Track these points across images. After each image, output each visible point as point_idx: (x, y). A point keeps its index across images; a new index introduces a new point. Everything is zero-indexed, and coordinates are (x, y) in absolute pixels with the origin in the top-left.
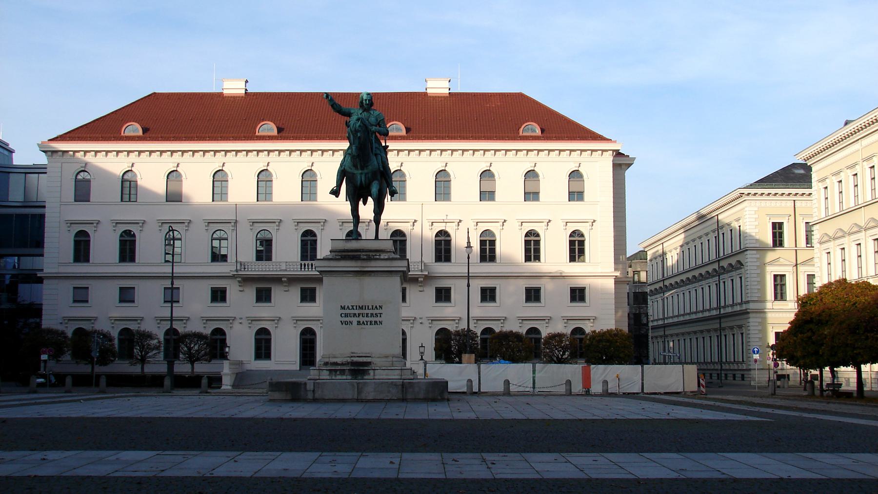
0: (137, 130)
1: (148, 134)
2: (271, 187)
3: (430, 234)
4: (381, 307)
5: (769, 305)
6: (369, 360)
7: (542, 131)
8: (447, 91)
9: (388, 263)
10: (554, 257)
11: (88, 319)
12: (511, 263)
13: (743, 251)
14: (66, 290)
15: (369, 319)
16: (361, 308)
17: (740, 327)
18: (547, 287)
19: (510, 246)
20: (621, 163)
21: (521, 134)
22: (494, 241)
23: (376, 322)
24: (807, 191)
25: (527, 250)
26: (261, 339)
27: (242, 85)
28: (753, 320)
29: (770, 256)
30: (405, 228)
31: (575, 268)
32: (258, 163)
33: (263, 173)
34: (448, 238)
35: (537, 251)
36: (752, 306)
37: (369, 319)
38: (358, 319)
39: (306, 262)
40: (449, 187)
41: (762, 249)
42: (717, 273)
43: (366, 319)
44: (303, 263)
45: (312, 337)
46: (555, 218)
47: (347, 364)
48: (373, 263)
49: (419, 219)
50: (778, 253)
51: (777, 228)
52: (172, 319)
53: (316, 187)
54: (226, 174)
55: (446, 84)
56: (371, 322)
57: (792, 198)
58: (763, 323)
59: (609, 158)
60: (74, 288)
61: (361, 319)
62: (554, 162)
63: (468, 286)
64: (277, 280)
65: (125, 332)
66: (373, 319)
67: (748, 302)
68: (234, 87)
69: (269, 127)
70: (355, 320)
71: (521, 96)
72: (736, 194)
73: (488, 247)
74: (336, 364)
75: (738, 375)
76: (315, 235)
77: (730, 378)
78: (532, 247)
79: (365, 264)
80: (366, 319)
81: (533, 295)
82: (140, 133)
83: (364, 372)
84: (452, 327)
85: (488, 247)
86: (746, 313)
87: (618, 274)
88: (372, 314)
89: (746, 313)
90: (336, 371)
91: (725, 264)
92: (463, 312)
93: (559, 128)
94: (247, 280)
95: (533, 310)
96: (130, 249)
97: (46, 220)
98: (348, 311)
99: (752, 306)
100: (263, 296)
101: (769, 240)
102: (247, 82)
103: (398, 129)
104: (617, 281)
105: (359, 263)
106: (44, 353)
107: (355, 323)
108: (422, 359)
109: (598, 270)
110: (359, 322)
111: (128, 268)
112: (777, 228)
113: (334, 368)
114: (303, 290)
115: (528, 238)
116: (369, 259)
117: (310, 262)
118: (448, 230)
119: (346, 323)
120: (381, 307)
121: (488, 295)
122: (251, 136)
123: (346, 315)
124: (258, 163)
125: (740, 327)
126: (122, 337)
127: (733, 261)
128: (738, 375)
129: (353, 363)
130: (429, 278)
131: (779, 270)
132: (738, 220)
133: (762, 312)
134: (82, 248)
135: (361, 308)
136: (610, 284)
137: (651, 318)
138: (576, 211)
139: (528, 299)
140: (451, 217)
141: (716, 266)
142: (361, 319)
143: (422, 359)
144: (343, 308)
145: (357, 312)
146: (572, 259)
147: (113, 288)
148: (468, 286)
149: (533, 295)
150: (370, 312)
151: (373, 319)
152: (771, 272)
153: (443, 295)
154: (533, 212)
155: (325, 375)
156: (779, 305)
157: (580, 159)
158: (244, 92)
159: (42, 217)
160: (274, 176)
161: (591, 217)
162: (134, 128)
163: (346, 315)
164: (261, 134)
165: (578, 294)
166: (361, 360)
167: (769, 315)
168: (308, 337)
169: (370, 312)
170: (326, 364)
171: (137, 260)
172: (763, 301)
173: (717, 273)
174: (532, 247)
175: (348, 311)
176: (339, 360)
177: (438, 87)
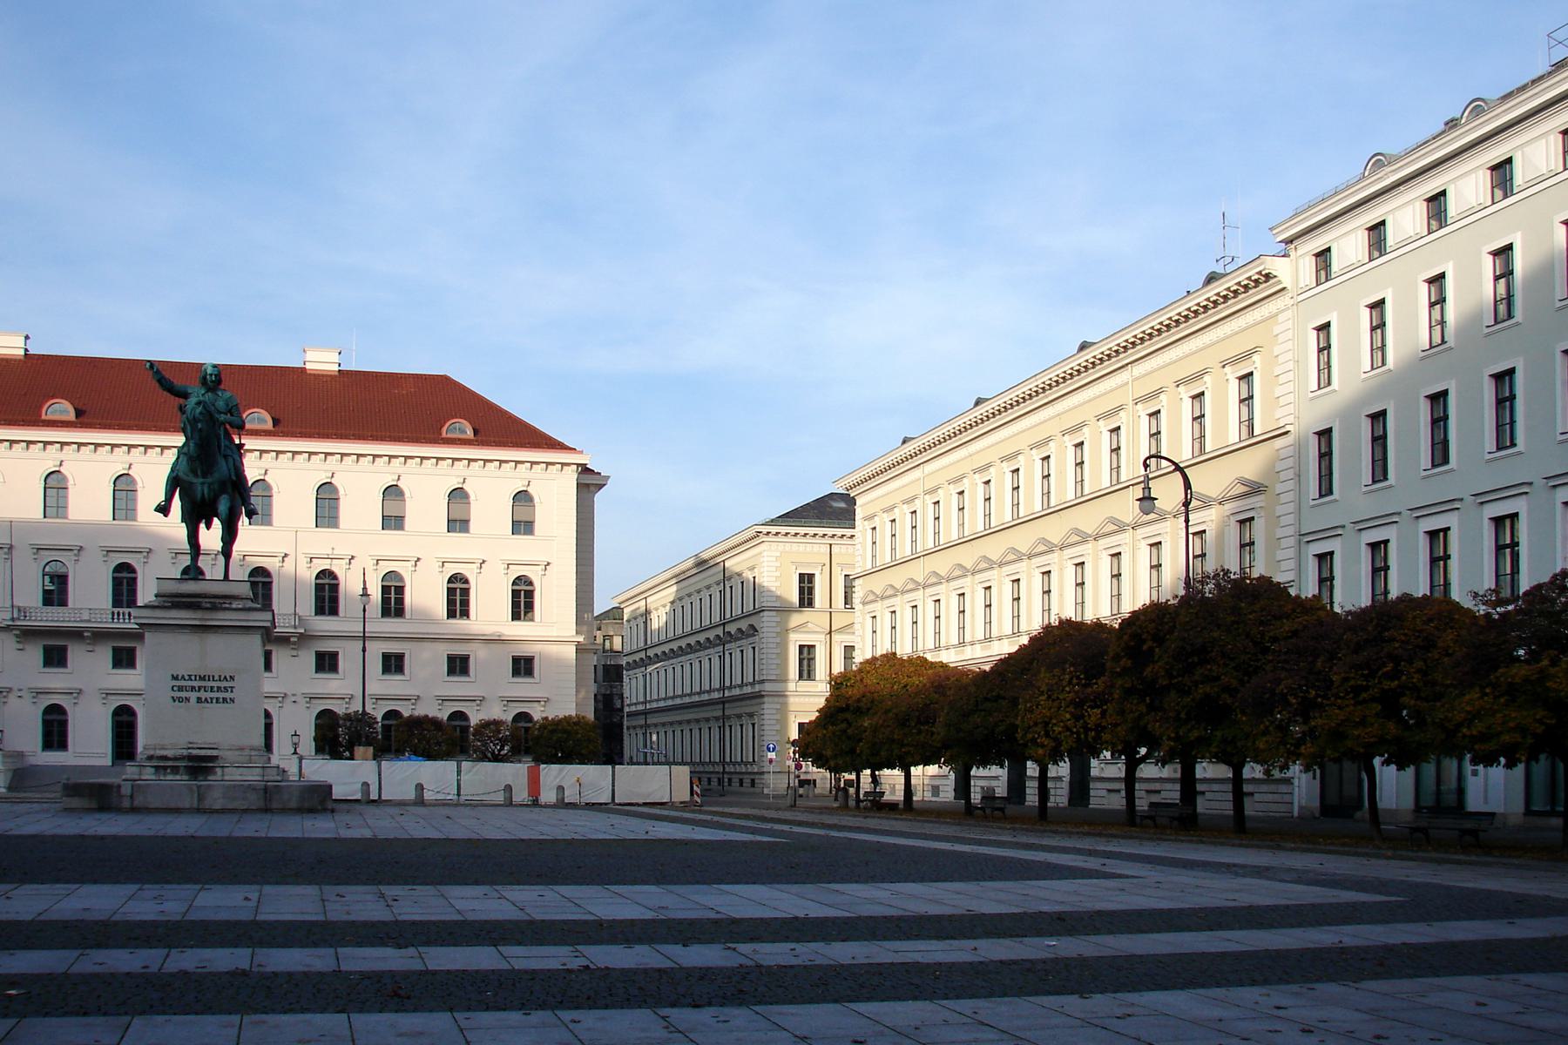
3: (308, 575)
5: (791, 686)
6: (214, 753)
7: (476, 432)
9: (242, 616)
10: (490, 611)
13: (758, 612)
16: (202, 678)
17: (751, 715)
18: (478, 654)
19: (427, 595)
20: (589, 483)
23: (225, 700)
24: (848, 532)
28: (769, 707)
29: (795, 620)
30: (271, 564)
31: (521, 629)
36: (768, 687)
40: (337, 508)
41: (784, 610)
42: (720, 641)
43: (209, 695)
46: (492, 559)
47: (182, 758)
48: (221, 615)
50: (807, 615)
51: (806, 582)
57: (828, 541)
58: (783, 711)
61: (203, 695)
62: (491, 478)
64: (76, 635)
66: (221, 695)
67: (762, 682)
70: (193, 696)
72: (751, 533)
74: (165, 758)
75: (747, 782)
76: (133, 571)
77: (736, 783)
78: (458, 598)
79: (208, 615)
80: (209, 695)
81: (459, 665)
83: (210, 770)
84: (340, 709)
86: (759, 696)
87: (581, 639)
88: (219, 689)
89: (759, 696)
90: (165, 768)
91: (732, 628)
92: (355, 688)
93: (501, 429)
95: (459, 687)
99: (768, 687)
100: (55, 658)
101: (795, 598)
102: (27, 338)
104: (580, 649)
105: (199, 614)
107: (193, 700)
109: (553, 633)
110: (199, 700)
112: (806, 582)
113: (163, 764)
116: (214, 608)
117: (127, 610)
118: (334, 569)
119: (180, 700)
123: (181, 689)
125: (751, 715)
127: (744, 625)
128: (747, 782)
129: (191, 758)
130: (305, 638)
131: (807, 639)
132: (752, 569)
133: (782, 695)
135: (202, 678)
136: (570, 652)
137: (627, 702)
138: (523, 548)
139: (452, 671)
141: (719, 631)
142: (203, 695)
144: (175, 678)
145: (196, 684)
146: (516, 616)
149: (459, 665)
151: (221, 695)
152: (795, 640)
153: (327, 663)
155: (149, 774)
156: (805, 685)
158: (22, 352)
163: (181, 689)
165: (523, 666)
167: (791, 700)
168: (125, 718)
170: (150, 758)
172: (785, 681)
173: (720, 641)
174: (458, 598)
176: (169, 753)
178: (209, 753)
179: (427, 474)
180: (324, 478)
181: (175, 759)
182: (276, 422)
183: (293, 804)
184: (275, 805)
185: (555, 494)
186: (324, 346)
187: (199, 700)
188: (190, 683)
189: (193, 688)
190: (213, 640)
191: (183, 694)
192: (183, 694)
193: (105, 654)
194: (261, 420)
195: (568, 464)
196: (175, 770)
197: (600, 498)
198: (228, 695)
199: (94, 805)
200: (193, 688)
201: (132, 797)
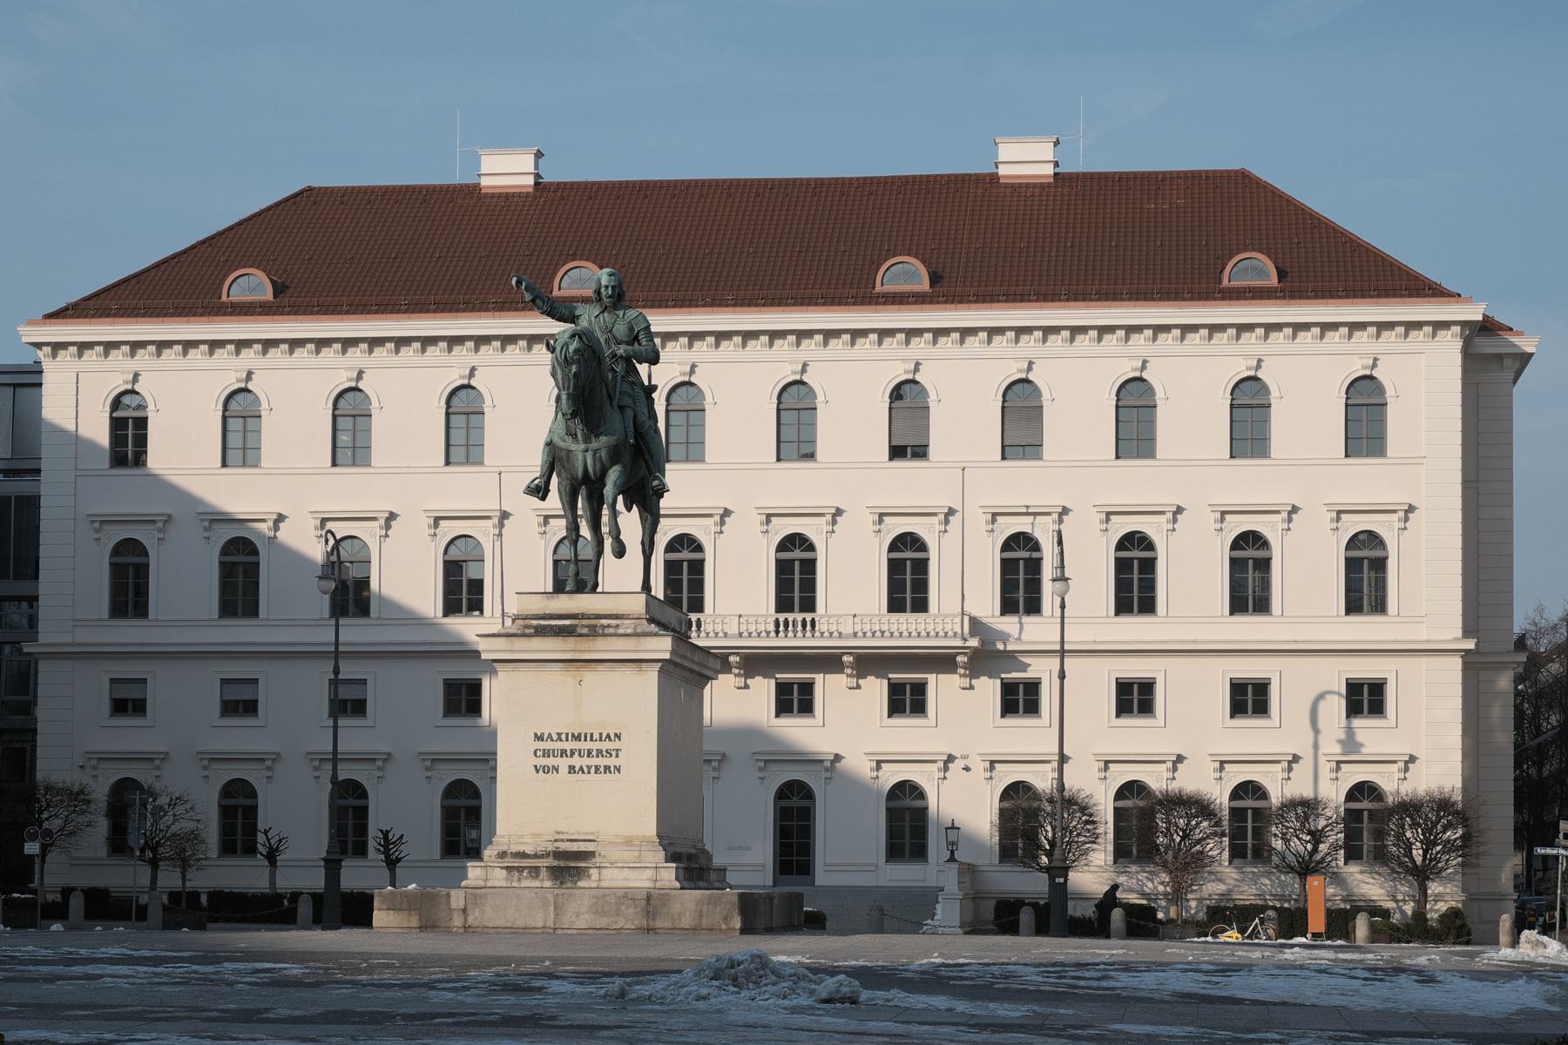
0: (1267, 275)
1: (289, 299)
2: (813, 424)
4: (618, 736)
6: (590, 847)
7: (1282, 275)
8: (1049, 170)
11: (147, 759)
12: (414, 620)
14: (94, 688)
15: (594, 761)
16: (577, 738)
19: (407, 579)
20: (1490, 360)
21: (1225, 282)
22: (813, 562)
23: (607, 768)
25: (1008, 586)
26: (235, 807)
27: (526, 162)
32: (225, 371)
33: (682, 390)
34: (1035, 555)
35: (1149, 586)
37: (594, 761)
38: (570, 761)
39: (790, 616)
40: (1152, 422)
43: (585, 761)
44: (782, 617)
45: (804, 803)
48: (600, 643)
49: (957, 506)
52: (335, 759)
53: (813, 424)
54: (811, 391)
55: (1045, 151)
56: (597, 768)
59: (1450, 349)
60: (112, 681)
61: (577, 761)
62: (1308, 360)
63: (1062, 676)
64: (829, 662)
65: (124, 788)
66: (602, 762)
68: (506, 170)
69: (1263, 268)
70: (563, 763)
71: (308, 196)
73: (1136, 576)
76: (923, 547)
80: (585, 761)
82: (268, 295)
83: (580, 873)
85: (1136, 576)
87: (1470, 645)
88: (599, 752)
90: (520, 869)
93: (1329, 264)
94: (868, 663)
96: (137, 585)
97: (44, 513)
98: (548, 745)
100: (907, 702)
102: (539, 155)
103: (912, 276)
106: (33, 838)
107: (564, 769)
108: (952, 859)
109: (1421, 635)
110: (572, 769)
111: (241, 632)
113: (519, 863)
114: (895, 690)
115: (1239, 554)
116: (594, 633)
117: (799, 617)
118: (1038, 534)
120: (618, 736)
121: (1249, 699)
122: (868, 298)
123: (546, 753)
124: (225, 371)
126: (1006, 805)
129: (558, 855)
134: (130, 586)
135: (577, 738)
138: (1367, 483)
140: (1036, 501)
142: (577, 761)
143: (952, 859)
144: (539, 738)
145: (568, 746)
147: (204, 686)
148: (1062, 676)
150: (594, 746)
151: (602, 762)
154: (911, 489)
157: (1376, 347)
158: (530, 181)
159: (31, 504)
160: (488, 402)
161: (1402, 498)
162: (252, 284)
163: (546, 753)
164: (889, 288)
166: (574, 847)
168: (795, 802)
169: (594, 746)
171: (262, 614)
175: (548, 745)
177: (1026, 158)
178: (583, 847)
179: (1193, 361)
180: (1128, 370)
181: (536, 856)
182: (935, 279)
183: (686, 922)
184: (659, 924)
185: (1425, 381)
186: (1024, 130)
187: (572, 769)
188: (559, 745)
189: (563, 753)
190: (592, 677)
191: (550, 762)
192: (550, 762)
193: (876, 689)
194: (912, 276)
195: (1446, 325)
196: (534, 872)
197: (1524, 391)
198: (612, 762)
199: (415, 922)
200: (563, 753)
201: (464, 910)
